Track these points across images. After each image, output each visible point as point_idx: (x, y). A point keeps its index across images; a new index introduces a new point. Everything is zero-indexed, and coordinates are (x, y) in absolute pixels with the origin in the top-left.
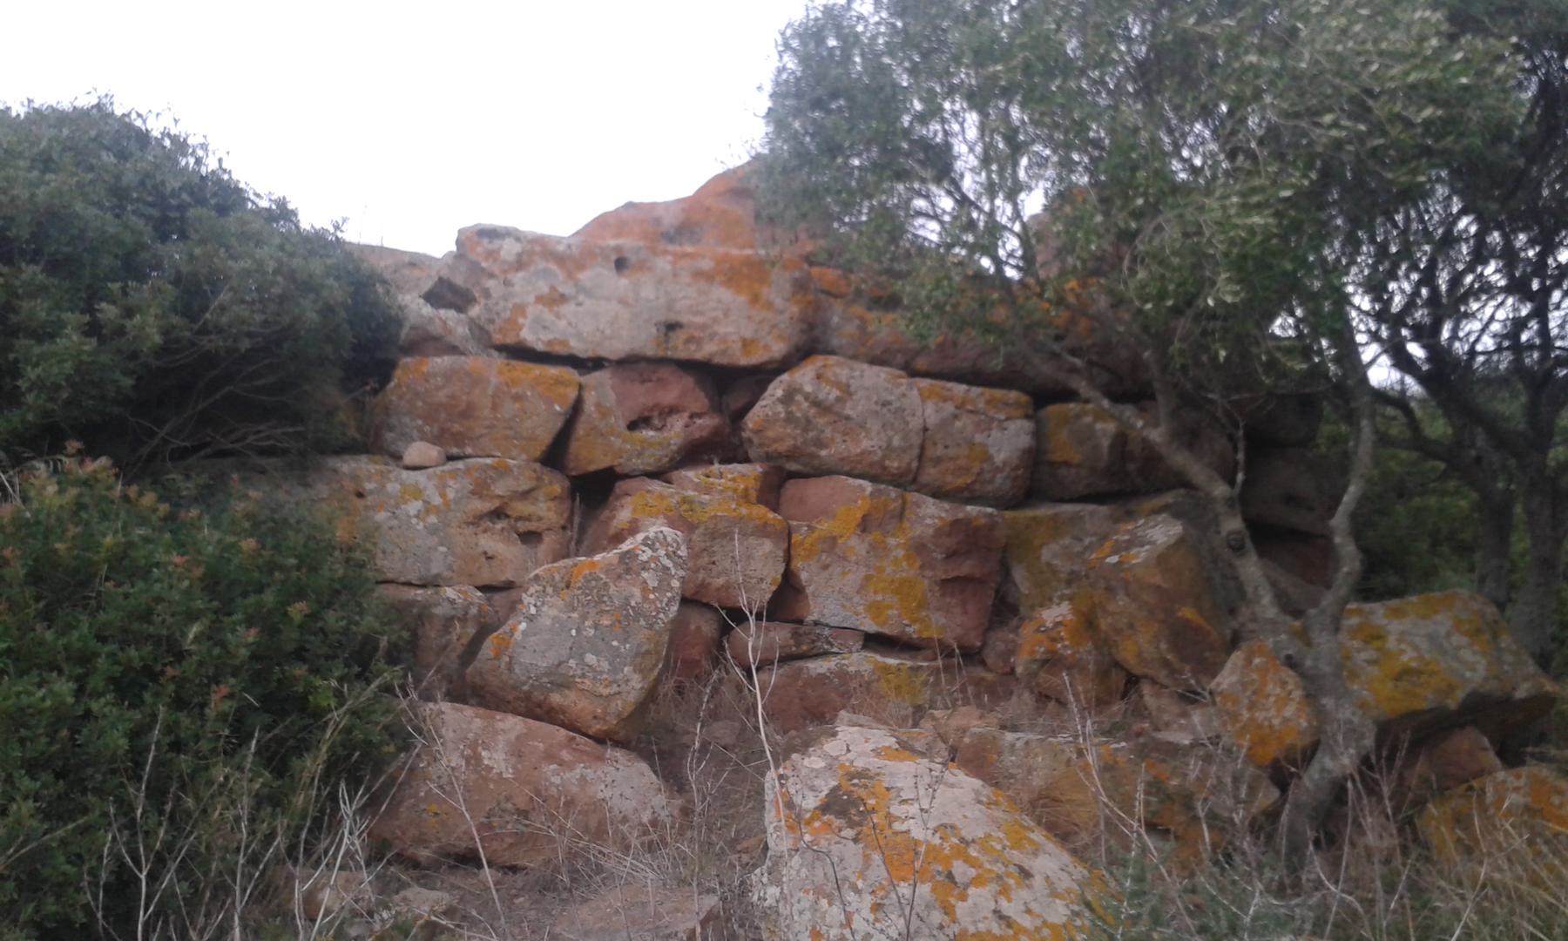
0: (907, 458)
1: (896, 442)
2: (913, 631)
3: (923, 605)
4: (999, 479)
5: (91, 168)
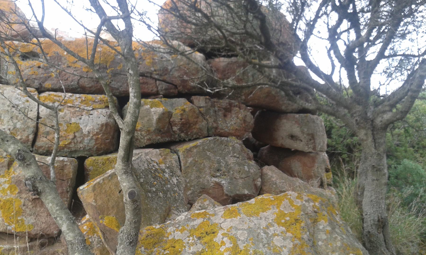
0: (25, 134)
1: (19, 125)
2: (12, 228)
3: (19, 213)
4: (86, 140)
5: (55, 58)
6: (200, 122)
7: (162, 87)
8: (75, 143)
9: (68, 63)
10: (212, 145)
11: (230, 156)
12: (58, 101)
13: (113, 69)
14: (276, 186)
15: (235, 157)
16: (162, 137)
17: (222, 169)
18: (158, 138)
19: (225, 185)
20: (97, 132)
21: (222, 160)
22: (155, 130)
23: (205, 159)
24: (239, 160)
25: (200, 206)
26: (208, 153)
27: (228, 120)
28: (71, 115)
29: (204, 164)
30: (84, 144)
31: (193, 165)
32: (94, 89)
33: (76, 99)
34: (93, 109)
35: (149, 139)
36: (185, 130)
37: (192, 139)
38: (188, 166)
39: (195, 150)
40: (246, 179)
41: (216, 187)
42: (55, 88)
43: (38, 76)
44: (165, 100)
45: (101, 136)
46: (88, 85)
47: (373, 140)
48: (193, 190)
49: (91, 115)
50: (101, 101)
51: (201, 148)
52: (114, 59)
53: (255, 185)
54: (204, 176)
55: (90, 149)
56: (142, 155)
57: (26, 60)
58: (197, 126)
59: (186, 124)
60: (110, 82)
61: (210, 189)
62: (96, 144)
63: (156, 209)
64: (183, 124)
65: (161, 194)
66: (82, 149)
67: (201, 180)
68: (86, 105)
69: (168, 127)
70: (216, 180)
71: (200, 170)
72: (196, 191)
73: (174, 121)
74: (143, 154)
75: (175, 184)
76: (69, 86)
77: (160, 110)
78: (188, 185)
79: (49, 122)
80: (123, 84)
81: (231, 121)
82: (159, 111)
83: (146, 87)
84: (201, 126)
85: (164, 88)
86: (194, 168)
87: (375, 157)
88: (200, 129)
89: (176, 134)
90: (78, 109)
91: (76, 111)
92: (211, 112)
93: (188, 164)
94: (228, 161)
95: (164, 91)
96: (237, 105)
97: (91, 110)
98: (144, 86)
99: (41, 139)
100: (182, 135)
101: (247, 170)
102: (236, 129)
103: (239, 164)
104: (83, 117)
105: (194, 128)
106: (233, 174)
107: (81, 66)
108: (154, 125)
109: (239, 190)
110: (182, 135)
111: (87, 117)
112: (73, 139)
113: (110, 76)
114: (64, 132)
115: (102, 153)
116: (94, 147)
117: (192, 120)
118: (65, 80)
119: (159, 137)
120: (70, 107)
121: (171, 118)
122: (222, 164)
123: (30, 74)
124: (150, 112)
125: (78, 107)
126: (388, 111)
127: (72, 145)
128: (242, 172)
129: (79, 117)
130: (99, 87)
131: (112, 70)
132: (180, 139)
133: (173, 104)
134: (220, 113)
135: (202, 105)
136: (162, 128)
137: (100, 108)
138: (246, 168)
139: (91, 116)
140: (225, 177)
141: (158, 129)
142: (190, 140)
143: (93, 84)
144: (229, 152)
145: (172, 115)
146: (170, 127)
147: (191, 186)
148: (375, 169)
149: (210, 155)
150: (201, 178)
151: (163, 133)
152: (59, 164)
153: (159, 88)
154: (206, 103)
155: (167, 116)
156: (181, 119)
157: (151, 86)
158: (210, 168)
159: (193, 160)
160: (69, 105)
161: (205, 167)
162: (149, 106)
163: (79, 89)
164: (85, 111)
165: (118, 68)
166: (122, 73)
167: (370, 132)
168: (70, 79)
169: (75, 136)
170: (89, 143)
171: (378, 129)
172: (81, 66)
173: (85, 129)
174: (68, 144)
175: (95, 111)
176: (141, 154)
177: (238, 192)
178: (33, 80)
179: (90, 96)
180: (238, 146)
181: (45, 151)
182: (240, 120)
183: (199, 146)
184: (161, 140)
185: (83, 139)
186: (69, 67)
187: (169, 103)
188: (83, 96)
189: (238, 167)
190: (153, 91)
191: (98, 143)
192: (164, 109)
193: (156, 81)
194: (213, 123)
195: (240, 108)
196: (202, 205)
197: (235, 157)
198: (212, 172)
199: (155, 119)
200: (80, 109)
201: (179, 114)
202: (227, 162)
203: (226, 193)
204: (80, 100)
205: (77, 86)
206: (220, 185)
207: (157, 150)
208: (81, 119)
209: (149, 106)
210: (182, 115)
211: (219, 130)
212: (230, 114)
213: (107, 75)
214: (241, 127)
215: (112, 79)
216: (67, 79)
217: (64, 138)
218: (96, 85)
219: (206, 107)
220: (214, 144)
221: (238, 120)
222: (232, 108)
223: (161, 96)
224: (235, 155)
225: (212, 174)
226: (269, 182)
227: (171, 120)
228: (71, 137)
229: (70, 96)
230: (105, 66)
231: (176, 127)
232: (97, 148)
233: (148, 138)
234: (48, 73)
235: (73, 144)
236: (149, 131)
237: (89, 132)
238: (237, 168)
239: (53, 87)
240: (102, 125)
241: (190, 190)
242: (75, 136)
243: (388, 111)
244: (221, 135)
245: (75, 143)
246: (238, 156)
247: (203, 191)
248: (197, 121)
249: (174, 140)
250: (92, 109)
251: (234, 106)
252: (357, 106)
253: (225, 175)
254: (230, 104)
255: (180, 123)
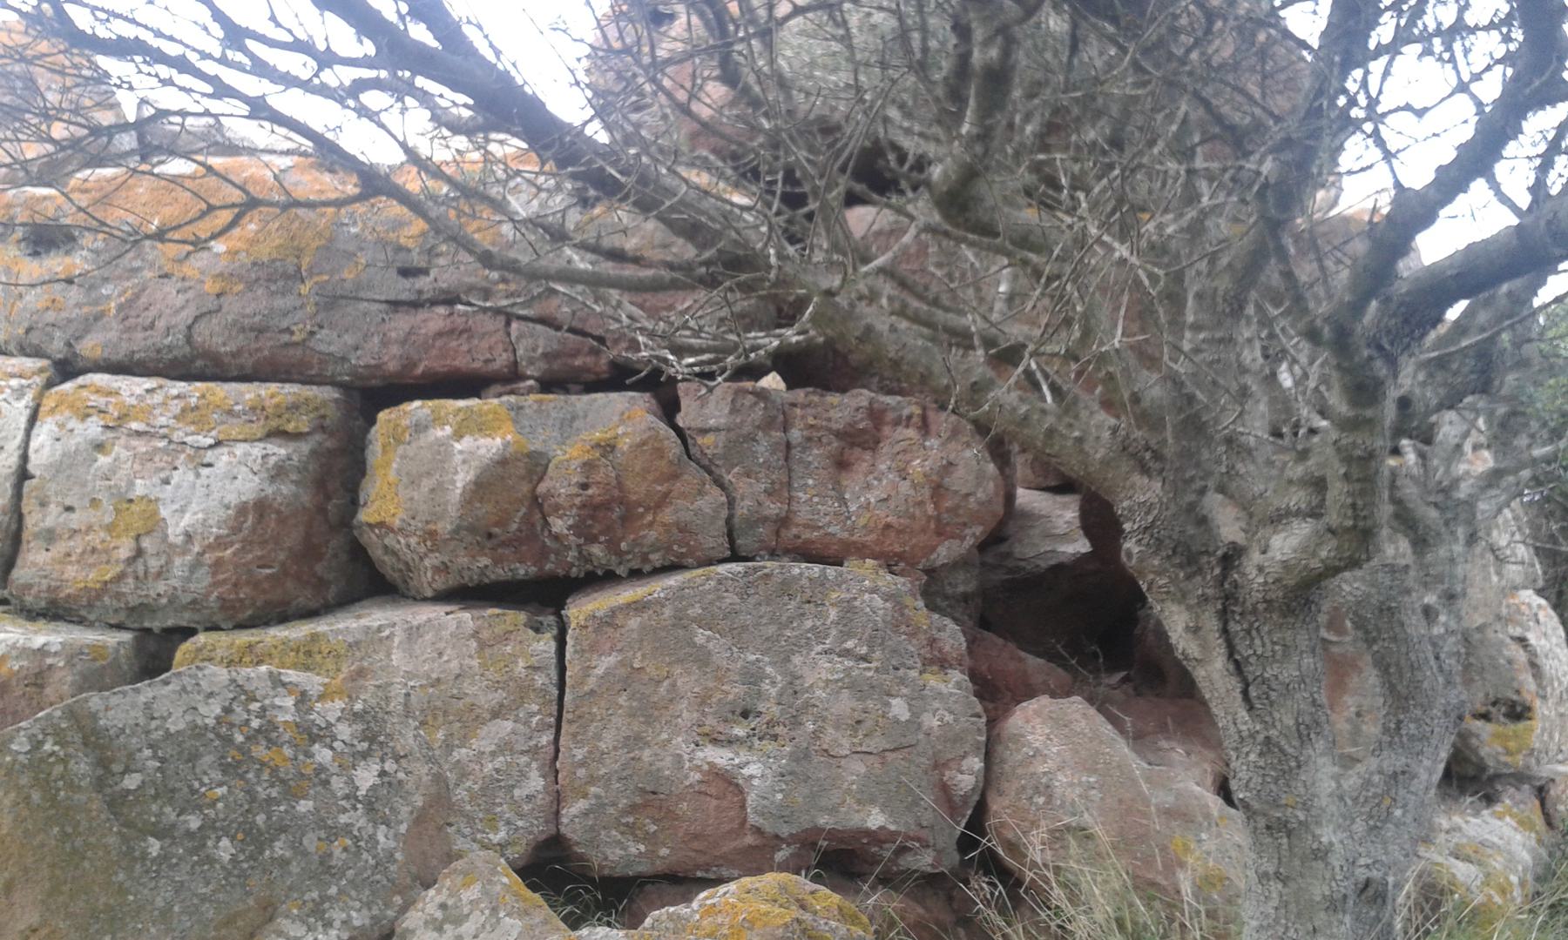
4: (180, 564)
6: (683, 495)
7: (534, 350)
8: (137, 578)
9: (163, 261)
10: (731, 598)
11: (819, 648)
12: (101, 412)
13: (326, 278)
14: (1050, 797)
15: (846, 653)
16: (497, 561)
17: (761, 707)
18: (481, 566)
19: (756, 782)
20: (218, 537)
21: (769, 670)
22: (457, 531)
23: (680, 661)
24: (867, 671)
25: (443, 906)
26: (701, 636)
27: (852, 484)
28: (137, 467)
29: (674, 685)
30: (174, 582)
31: (618, 687)
32: (248, 362)
33: (164, 404)
34: (218, 444)
35: (444, 568)
36: (601, 533)
37: (647, 568)
38: (592, 692)
39: (634, 623)
40: (890, 756)
41: (713, 791)
42: (114, 358)
43: (64, 315)
44: (540, 402)
45: (234, 554)
46: (224, 344)
47: (1231, 667)
48: (597, 797)
49: (209, 465)
50: (253, 409)
51: (668, 612)
52: (331, 240)
53: (945, 789)
54: (664, 736)
55: (194, 602)
56: (392, 634)
57: (48, 251)
58: (667, 515)
59: (606, 506)
60: (312, 333)
61: (681, 798)
62: (216, 584)
63: (166, 913)
64: (592, 510)
65: (225, 849)
66: (164, 601)
67: (646, 755)
68: (192, 428)
69: (527, 519)
70: (720, 757)
71: (649, 713)
72: (614, 804)
73: (549, 494)
74: (398, 630)
75: (362, 793)
76: (158, 351)
77: (489, 446)
78: (581, 772)
79: (56, 494)
80: (366, 337)
81: (868, 487)
82: (483, 451)
83: (465, 348)
84: (686, 516)
85: (540, 350)
86: (622, 700)
87: (1252, 757)
88: (683, 528)
89: (568, 548)
90: (162, 444)
91: (156, 450)
92: (762, 448)
93: (591, 683)
94: (806, 671)
95: (542, 365)
96: (909, 417)
97: (211, 447)
98: (454, 344)
99: (31, 557)
100: (597, 550)
101: (905, 716)
102: (888, 526)
103: (856, 687)
104: (176, 477)
105: (651, 525)
106: (816, 735)
107: (202, 273)
108: (453, 511)
109: (833, 810)
110: (597, 550)
111: (191, 476)
112: (131, 561)
113: (310, 309)
114: (102, 534)
115: (251, 617)
116: (207, 595)
117: (637, 489)
118: (145, 329)
119: (484, 561)
120: (139, 434)
121: (541, 479)
122: (766, 685)
123: (39, 306)
124: (449, 454)
125: (164, 437)
126: (1297, 513)
127: (128, 586)
128: (869, 724)
129: (163, 475)
130: (266, 353)
131: (321, 286)
132: (589, 567)
133: (574, 418)
134: (815, 455)
135: (712, 422)
136: (497, 524)
137: (245, 441)
138: (899, 708)
139: (205, 471)
140: (769, 746)
141: (472, 529)
142: (636, 574)
143: (241, 340)
144: (821, 635)
145: (547, 467)
146: (538, 516)
147: (592, 780)
148: (1262, 822)
149: (711, 645)
150: (647, 744)
151: (503, 544)
152: (25, 663)
153: (520, 352)
154: (734, 411)
155: (522, 472)
156: (585, 486)
157: (485, 344)
158: (703, 700)
159: (622, 663)
160: (134, 426)
161: (674, 696)
162: (448, 430)
163: (199, 363)
164: (189, 451)
165: (346, 275)
166: (362, 294)
167: (1211, 623)
168: (161, 324)
169: (139, 552)
170: (188, 579)
171: (1254, 611)
172: (202, 273)
173: (177, 524)
174: (111, 581)
175: (225, 450)
176: (387, 633)
177: (824, 820)
178: (49, 329)
179: (222, 391)
180: (878, 601)
181: (43, 604)
182: (914, 486)
183: (660, 603)
184: (500, 573)
185: (169, 562)
186: (166, 276)
187: (554, 414)
188: (194, 390)
189: (854, 704)
190: (496, 366)
191: (225, 581)
192: (506, 445)
193: (508, 324)
194: (762, 497)
195: (925, 427)
196: (450, 902)
197: (846, 653)
198: (711, 721)
199: (459, 485)
200: (170, 442)
201: (574, 464)
202: (794, 678)
203: (753, 819)
204: (176, 407)
205: (187, 349)
206: (730, 783)
207: (466, 616)
208: (166, 482)
209: (448, 430)
210: (589, 466)
211: (794, 531)
212: (868, 456)
213: (298, 303)
214: (913, 517)
215: (319, 319)
216: (153, 323)
217: (104, 557)
218: (254, 346)
219: (729, 430)
220: (744, 595)
221: (905, 487)
222: (887, 430)
223: (531, 382)
224: (850, 644)
225: (707, 729)
226: (1020, 778)
227: (542, 488)
228: (124, 552)
229: (148, 391)
230: (291, 270)
231: (560, 517)
232: (220, 598)
233: (436, 562)
234: (96, 302)
235: (130, 580)
236: (432, 534)
237: (189, 537)
238: (845, 704)
239: (106, 355)
240: (242, 510)
241: (585, 796)
242: (139, 552)
243: (1297, 513)
244: (807, 554)
245: (137, 578)
246: (864, 650)
247: (645, 806)
248: (666, 495)
249: (561, 572)
250: (211, 441)
251: (897, 423)
252: (1138, 479)
253: (775, 737)
254: (876, 415)
255: (577, 501)
